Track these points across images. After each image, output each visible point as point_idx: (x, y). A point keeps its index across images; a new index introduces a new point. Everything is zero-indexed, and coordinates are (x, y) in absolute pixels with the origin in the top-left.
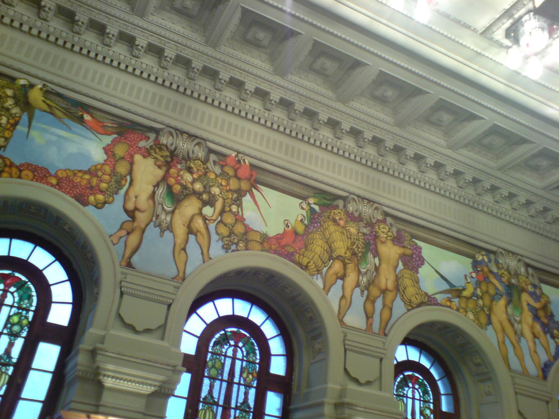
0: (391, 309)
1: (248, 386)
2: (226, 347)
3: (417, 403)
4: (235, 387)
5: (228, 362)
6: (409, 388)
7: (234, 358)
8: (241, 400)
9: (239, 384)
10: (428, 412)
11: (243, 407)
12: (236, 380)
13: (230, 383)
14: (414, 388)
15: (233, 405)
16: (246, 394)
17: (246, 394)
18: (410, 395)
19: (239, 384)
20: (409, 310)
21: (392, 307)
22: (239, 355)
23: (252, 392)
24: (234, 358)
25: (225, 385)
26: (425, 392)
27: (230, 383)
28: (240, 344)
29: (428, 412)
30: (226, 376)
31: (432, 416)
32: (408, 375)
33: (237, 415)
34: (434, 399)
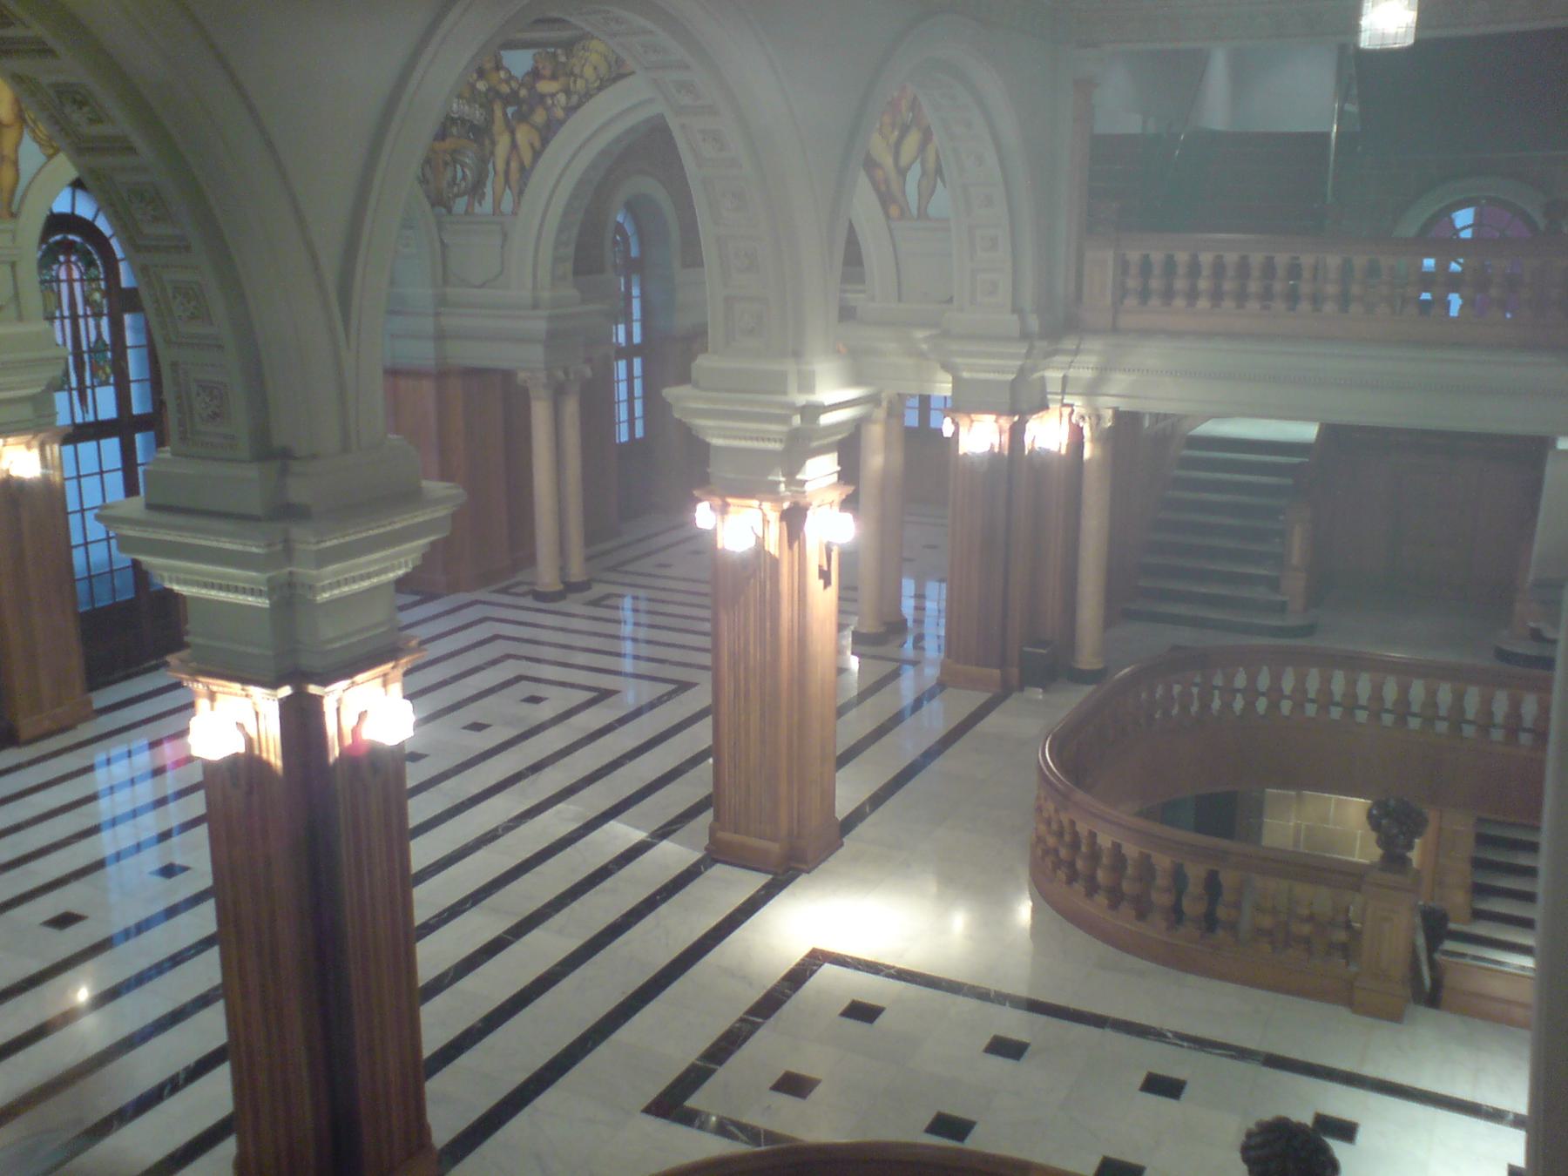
0: (15, 163)
1: (97, 315)
2: (55, 267)
3: (77, 286)
4: (81, 322)
5: (64, 287)
6: (61, 264)
7: (70, 281)
8: (93, 337)
9: (86, 316)
10: (97, 296)
11: (97, 348)
12: (80, 311)
13: (74, 318)
14: (68, 262)
15: (85, 348)
16: (98, 327)
17: (98, 327)
18: (63, 275)
19: (86, 316)
20: (50, 157)
21: (562, 123)
22: (76, 275)
23: (105, 322)
24: (70, 281)
25: (67, 322)
26: (90, 263)
27: (74, 318)
28: (73, 258)
29: (97, 296)
30: (66, 313)
31: (105, 302)
32: (57, 243)
33: (621, 328)
34: (106, 272)
